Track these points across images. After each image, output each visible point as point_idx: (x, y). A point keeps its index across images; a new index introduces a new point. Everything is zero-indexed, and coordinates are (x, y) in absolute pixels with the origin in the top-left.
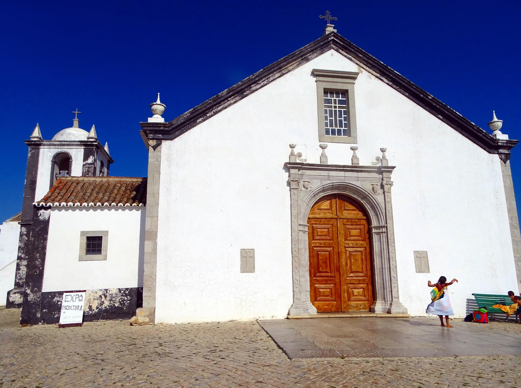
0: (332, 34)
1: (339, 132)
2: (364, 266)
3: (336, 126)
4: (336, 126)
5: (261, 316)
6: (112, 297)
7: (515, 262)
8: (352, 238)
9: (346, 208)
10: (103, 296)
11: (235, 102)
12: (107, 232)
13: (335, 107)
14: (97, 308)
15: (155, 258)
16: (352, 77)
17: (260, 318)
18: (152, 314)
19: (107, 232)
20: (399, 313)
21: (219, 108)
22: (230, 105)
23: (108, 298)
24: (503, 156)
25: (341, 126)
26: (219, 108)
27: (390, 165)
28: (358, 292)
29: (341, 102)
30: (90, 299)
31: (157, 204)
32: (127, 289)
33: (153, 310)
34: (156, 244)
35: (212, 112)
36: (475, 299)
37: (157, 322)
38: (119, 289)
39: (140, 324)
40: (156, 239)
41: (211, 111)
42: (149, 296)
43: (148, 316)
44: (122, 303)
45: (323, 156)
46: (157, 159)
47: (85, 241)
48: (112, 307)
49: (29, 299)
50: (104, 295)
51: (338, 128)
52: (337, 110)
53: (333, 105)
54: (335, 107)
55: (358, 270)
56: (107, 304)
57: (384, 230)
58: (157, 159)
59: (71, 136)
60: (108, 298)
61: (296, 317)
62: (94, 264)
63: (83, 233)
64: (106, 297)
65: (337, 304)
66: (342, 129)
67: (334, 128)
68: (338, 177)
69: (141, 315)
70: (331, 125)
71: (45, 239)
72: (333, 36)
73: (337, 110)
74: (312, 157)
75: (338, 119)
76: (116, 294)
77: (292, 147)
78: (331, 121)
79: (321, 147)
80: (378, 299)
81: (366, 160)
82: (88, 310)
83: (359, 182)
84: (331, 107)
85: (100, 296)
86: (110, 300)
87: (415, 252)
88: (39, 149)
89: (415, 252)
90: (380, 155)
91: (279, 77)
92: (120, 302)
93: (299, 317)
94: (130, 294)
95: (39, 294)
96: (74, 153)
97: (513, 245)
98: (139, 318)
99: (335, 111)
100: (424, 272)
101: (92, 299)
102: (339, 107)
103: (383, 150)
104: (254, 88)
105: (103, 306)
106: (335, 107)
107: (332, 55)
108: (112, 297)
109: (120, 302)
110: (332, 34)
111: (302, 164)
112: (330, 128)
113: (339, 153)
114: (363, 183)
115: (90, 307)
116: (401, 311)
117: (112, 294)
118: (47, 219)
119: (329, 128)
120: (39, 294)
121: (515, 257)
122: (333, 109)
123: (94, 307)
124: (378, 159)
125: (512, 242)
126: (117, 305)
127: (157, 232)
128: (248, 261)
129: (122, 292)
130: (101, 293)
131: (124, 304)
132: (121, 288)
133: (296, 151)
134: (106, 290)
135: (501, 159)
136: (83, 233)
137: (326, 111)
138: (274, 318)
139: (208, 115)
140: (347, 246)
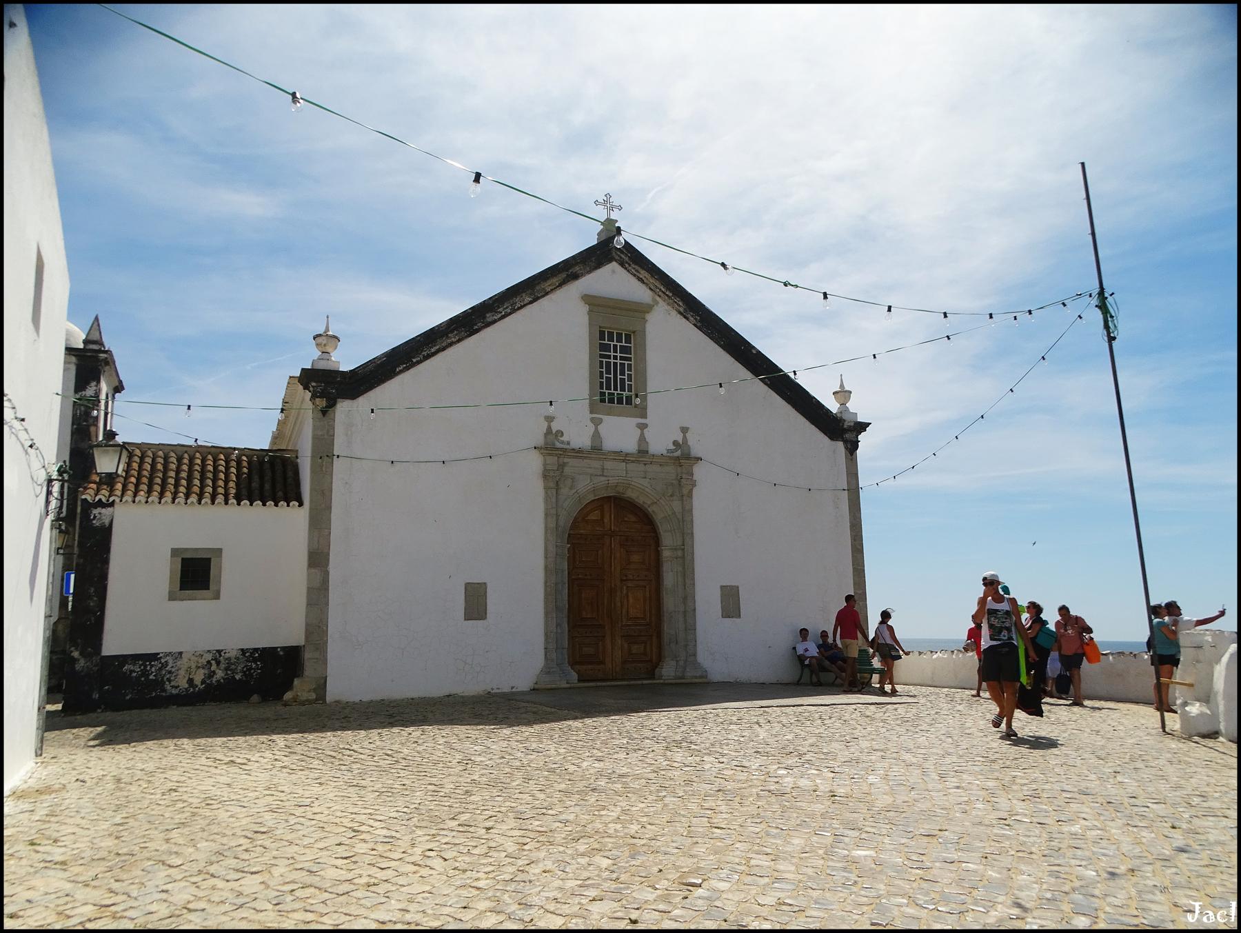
1: (620, 401)
3: (616, 389)
4: (616, 389)
6: (230, 664)
11: (459, 341)
12: (220, 550)
13: (615, 358)
14: (203, 682)
15: (327, 596)
18: (321, 687)
19: (220, 550)
22: (451, 345)
23: (223, 666)
25: (623, 389)
31: (330, 508)
32: (256, 650)
34: (327, 573)
36: (1052, 626)
37: (329, 699)
39: (303, 704)
43: (315, 690)
44: (247, 673)
45: (596, 436)
48: (230, 681)
49: (78, 667)
50: (215, 659)
52: (616, 372)
54: (615, 357)
56: (220, 674)
62: (197, 608)
63: (175, 552)
64: (218, 663)
68: (617, 471)
69: (301, 688)
70: (608, 388)
71: (106, 562)
73: (616, 372)
74: (578, 434)
76: (237, 658)
77: (550, 419)
79: (592, 420)
81: (660, 443)
84: (609, 357)
85: (209, 662)
86: (226, 669)
87: (722, 587)
88: (546, 443)
89: (722, 587)
91: (531, 303)
94: (260, 658)
95: (96, 659)
99: (615, 364)
102: (622, 358)
103: (684, 430)
104: (489, 320)
105: (214, 680)
106: (615, 358)
107: (613, 272)
108: (230, 664)
111: (565, 450)
113: (619, 432)
114: (643, 487)
115: (191, 681)
117: (229, 659)
120: (96, 659)
124: (675, 443)
126: (238, 677)
128: (476, 602)
130: (209, 657)
131: (251, 675)
134: (219, 652)
135: (846, 448)
136: (175, 552)
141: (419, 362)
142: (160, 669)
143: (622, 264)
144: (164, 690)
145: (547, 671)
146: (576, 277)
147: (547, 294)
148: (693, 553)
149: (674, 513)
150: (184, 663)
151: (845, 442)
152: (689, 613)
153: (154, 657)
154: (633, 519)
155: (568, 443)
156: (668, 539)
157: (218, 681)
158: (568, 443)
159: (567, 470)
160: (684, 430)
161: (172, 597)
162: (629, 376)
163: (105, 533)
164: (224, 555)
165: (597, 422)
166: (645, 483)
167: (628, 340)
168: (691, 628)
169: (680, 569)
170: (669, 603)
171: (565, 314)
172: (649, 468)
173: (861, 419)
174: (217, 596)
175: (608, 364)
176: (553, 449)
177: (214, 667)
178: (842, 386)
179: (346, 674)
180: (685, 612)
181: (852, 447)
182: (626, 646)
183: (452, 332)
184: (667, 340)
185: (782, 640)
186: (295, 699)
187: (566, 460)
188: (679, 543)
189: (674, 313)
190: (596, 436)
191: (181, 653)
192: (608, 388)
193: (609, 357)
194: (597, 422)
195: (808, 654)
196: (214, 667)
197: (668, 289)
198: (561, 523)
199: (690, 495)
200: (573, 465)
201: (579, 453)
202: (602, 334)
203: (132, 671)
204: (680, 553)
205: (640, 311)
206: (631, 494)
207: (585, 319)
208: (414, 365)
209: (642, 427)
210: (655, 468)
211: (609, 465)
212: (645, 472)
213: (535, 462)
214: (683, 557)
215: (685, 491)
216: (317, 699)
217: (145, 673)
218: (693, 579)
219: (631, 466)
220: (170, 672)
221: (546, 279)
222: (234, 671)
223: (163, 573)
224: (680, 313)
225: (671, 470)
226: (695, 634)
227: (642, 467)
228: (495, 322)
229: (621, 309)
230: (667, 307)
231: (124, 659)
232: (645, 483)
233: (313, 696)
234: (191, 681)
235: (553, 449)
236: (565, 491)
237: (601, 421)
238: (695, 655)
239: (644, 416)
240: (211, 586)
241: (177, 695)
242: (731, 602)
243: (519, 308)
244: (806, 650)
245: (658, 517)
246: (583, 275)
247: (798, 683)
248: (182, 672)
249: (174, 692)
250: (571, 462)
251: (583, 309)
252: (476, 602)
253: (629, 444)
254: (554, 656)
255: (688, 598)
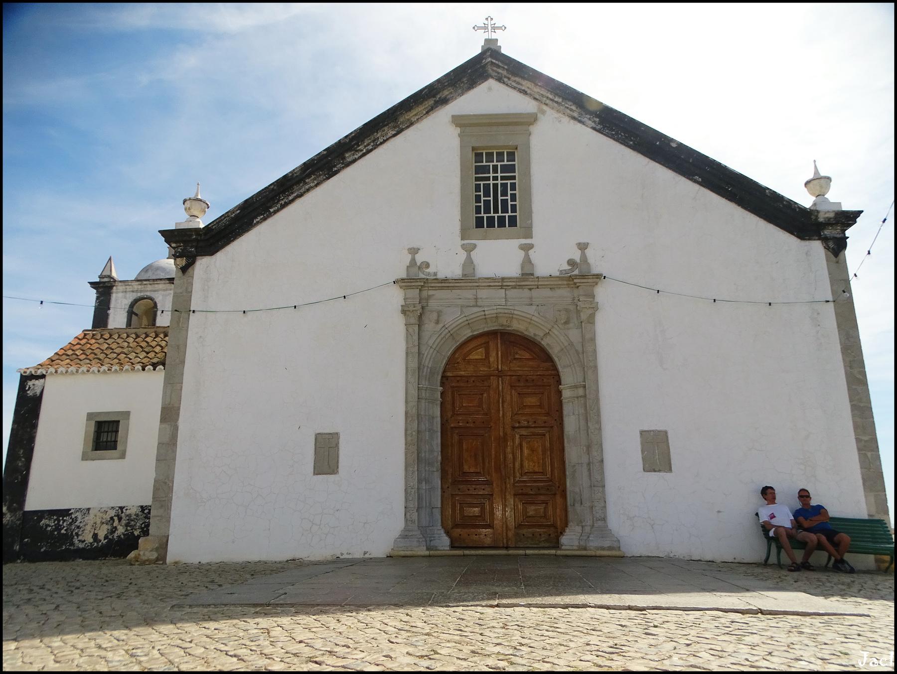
0: (489, 54)
1: (502, 224)
2: (548, 461)
3: (496, 211)
4: (496, 211)
5: (345, 552)
6: (130, 520)
7: (859, 450)
8: (527, 411)
9: (517, 356)
10: (116, 518)
11: (316, 186)
13: (495, 178)
14: (106, 537)
15: (174, 452)
16: (525, 122)
17: (342, 554)
18: (163, 546)
20: (603, 549)
21: (290, 198)
22: (308, 190)
23: (124, 522)
24: (831, 245)
25: (505, 210)
26: (290, 198)
27: (595, 271)
28: (535, 510)
29: (505, 169)
30: (95, 523)
33: (165, 541)
34: (176, 428)
35: (279, 206)
37: (170, 559)
38: (142, 507)
39: (143, 563)
40: (177, 420)
41: (277, 203)
42: (161, 516)
43: (157, 549)
45: (469, 263)
46: (187, 289)
47: (92, 429)
50: (118, 516)
51: (500, 214)
52: (495, 195)
53: (491, 175)
55: (537, 469)
56: (121, 530)
57: (409, 302)
58: (187, 289)
59: (159, 272)
60: (124, 522)
61: (402, 553)
62: (106, 467)
63: (90, 416)
64: (120, 519)
65: (494, 534)
66: (507, 215)
67: (492, 214)
69: (146, 548)
70: (487, 211)
72: (491, 56)
73: (495, 195)
74: (446, 262)
75: (500, 198)
76: (137, 515)
77: (414, 251)
78: (487, 203)
79: (463, 246)
80: (571, 524)
81: (550, 262)
82: (91, 540)
83: (534, 307)
84: (488, 179)
85: (112, 518)
86: (127, 525)
87: (642, 433)
89: (642, 433)
90: (576, 256)
91: (394, 135)
92: (142, 528)
93: (408, 553)
96: (161, 298)
97: (853, 416)
98: (141, 553)
99: (495, 186)
100: (659, 471)
101: (98, 522)
102: (503, 178)
104: (349, 160)
105: (116, 535)
107: (490, 89)
109: (142, 528)
110: (489, 54)
112: (485, 216)
114: (529, 316)
115: (95, 536)
116: (607, 544)
117: (129, 516)
118: (38, 394)
119: (482, 215)
120: (19, 514)
121: (858, 440)
122: (491, 175)
123: (101, 536)
124: (571, 263)
125: (852, 411)
127: (179, 409)
128: (326, 455)
129: (146, 511)
130: (112, 513)
132: (144, 505)
133: (420, 258)
134: (121, 508)
135: (827, 248)
136: (90, 416)
137: (478, 188)
138: (367, 556)
139: (272, 210)
140: (517, 425)
141: (275, 212)
142: (71, 524)
143: (500, 80)
144: (73, 544)
145: (404, 536)
146: (445, 101)
147: (412, 124)
148: (597, 391)
149: (571, 344)
150: (90, 519)
151: (825, 240)
152: (595, 465)
153: (66, 513)
154: (527, 356)
155: (435, 274)
156: (568, 377)
157: (119, 537)
158: (435, 274)
159: (433, 304)
160: (583, 247)
161: (85, 457)
162: (513, 197)
163: (37, 400)
164: (131, 416)
165: (469, 249)
166: (532, 310)
167: (511, 157)
168: (598, 485)
169: (582, 411)
170: (573, 454)
171: (436, 141)
172: (535, 293)
173: (848, 206)
174: (123, 456)
175: (487, 187)
176: (419, 285)
177: (116, 523)
178: (816, 171)
179: (193, 536)
180: (589, 464)
181: (838, 246)
182: (520, 506)
183: (309, 176)
184: (557, 154)
185: (742, 504)
186: (137, 559)
187: (431, 293)
188: (581, 379)
189: (566, 119)
190: (469, 263)
191: (89, 509)
192: (487, 211)
193: (488, 179)
194: (469, 249)
195: (774, 522)
196: (116, 523)
197: (556, 94)
198: (427, 362)
199: (591, 320)
200: (438, 299)
201: (445, 284)
202: (478, 157)
203: (48, 526)
204: (581, 392)
205: (522, 123)
206: (517, 326)
207: (456, 142)
208: (270, 215)
209: (527, 248)
210: (546, 292)
211: (483, 293)
212: (531, 298)
213: (396, 297)
214: (585, 396)
215: (584, 316)
216: (157, 559)
217: (58, 528)
218: (599, 422)
219: (512, 293)
220: (78, 527)
221: (410, 109)
222: (133, 527)
223: (79, 434)
224: (574, 118)
225: (565, 293)
226: (604, 492)
227: (526, 293)
228: (354, 161)
229: (501, 124)
230: (556, 115)
231: (41, 514)
232: (532, 310)
233: (154, 555)
234: (95, 536)
235: (419, 285)
236: (429, 326)
237: (475, 246)
238: (604, 519)
239: (529, 235)
240: (118, 447)
241: (83, 549)
242: (656, 452)
243: (381, 143)
244: (773, 516)
245: (554, 352)
246: (454, 98)
247: (765, 564)
248: (88, 528)
249: (81, 546)
250: (439, 294)
251: (455, 132)
252: (326, 455)
253: (511, 269)
254: (415, 516)
255: (593, 445)
